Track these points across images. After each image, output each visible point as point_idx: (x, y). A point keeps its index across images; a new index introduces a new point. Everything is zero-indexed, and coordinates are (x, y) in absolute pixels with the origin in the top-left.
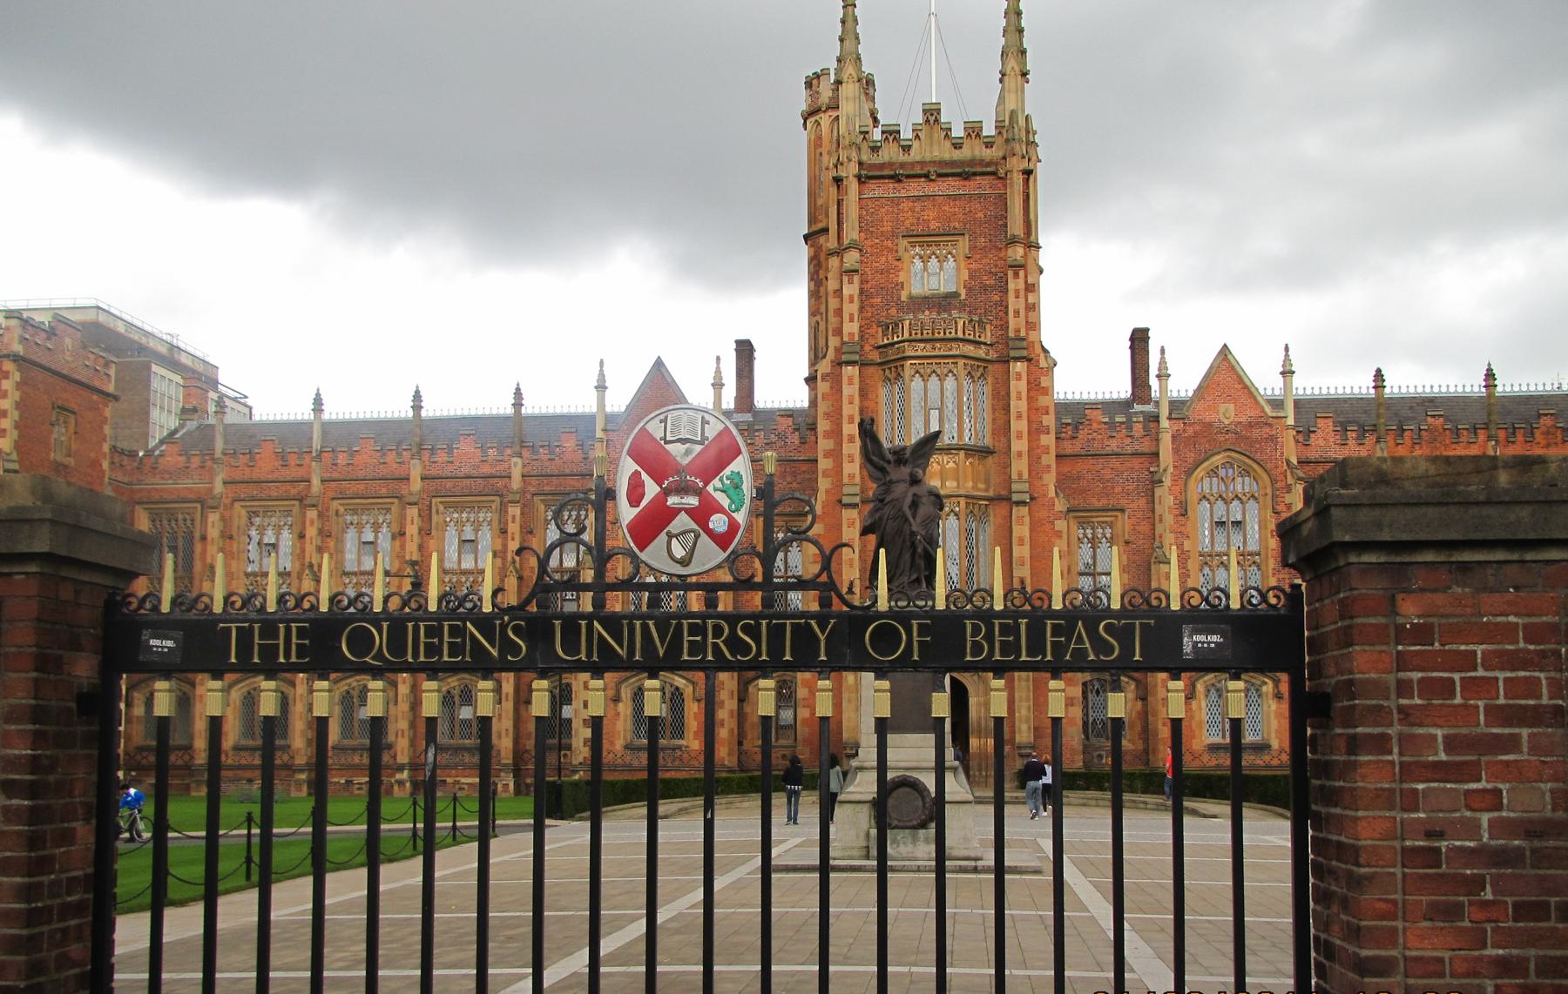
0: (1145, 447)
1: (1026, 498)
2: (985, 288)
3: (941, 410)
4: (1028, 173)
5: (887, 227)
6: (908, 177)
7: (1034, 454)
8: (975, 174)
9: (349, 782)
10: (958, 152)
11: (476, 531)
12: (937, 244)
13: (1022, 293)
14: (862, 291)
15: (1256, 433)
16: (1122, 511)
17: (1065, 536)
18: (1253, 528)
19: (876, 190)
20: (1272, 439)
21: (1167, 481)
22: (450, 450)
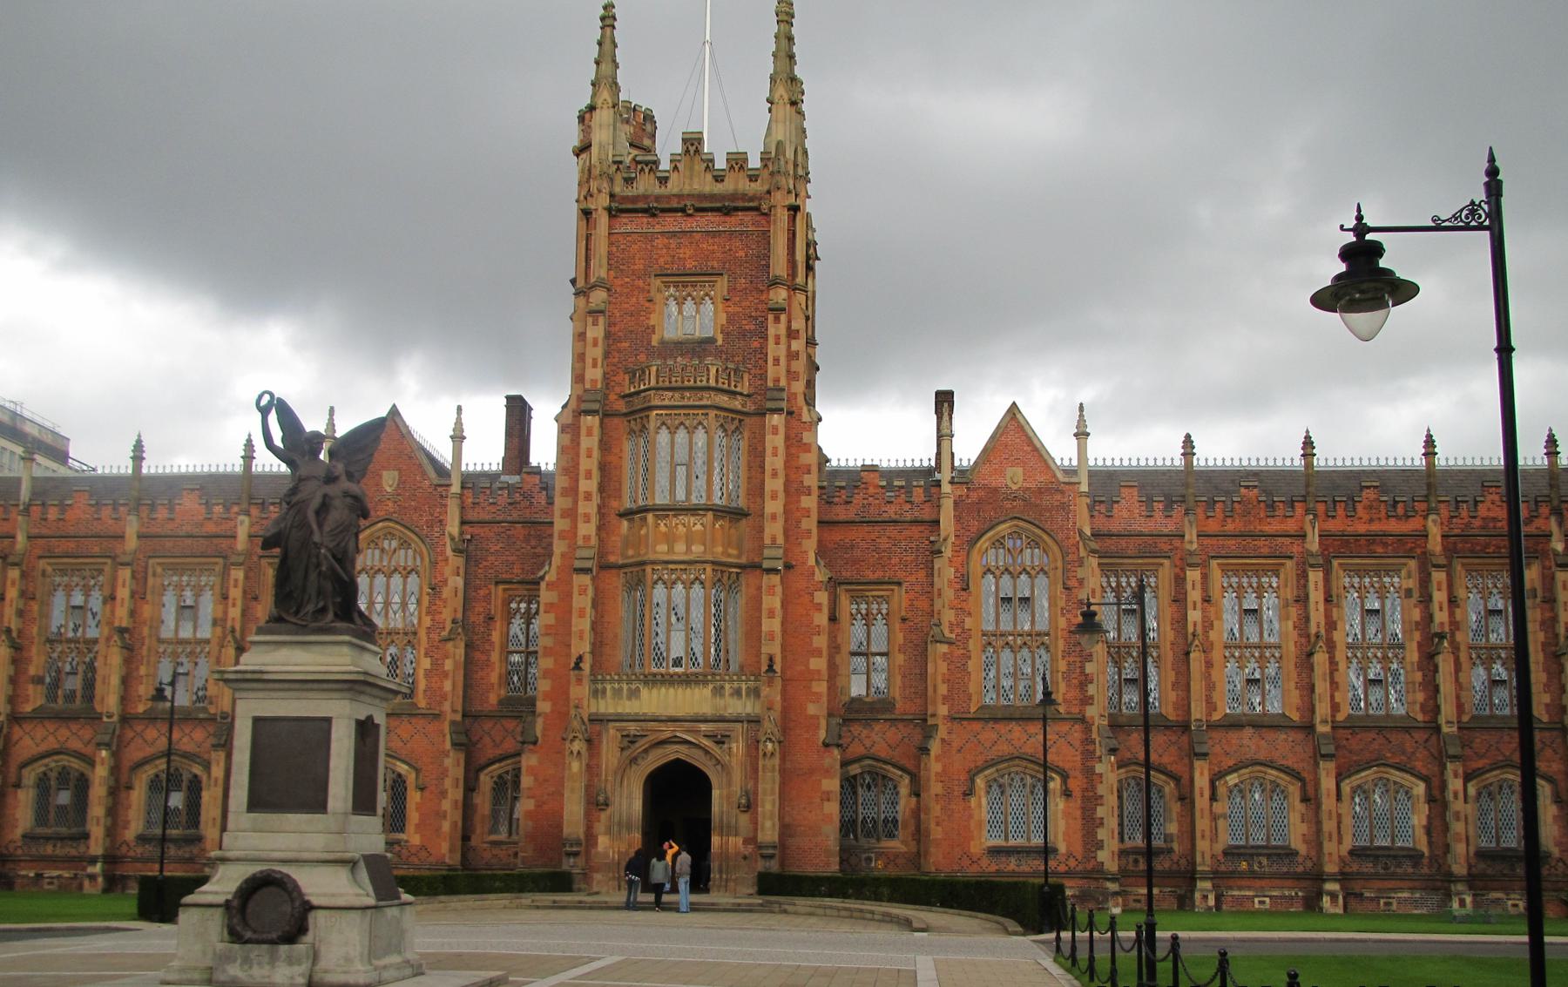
0: (927, 514)
2: (743, 334)
3: (689, 466)
4: (794, 209)
5: (639, 266)
6: (663, 210)
7: (791, 516)
8: (737, 209)
9: (39, 876)
10: (719, 186)
11: (197, 596)
12: (694, 284)
13: (783, 339)
14: (608, 335)
15: (1047, 501)
16: (899, 584)
18: (1042, 603)
19: (627, 224)
20: (1064, 507)
21: (948, 552)
22: (171, 509)
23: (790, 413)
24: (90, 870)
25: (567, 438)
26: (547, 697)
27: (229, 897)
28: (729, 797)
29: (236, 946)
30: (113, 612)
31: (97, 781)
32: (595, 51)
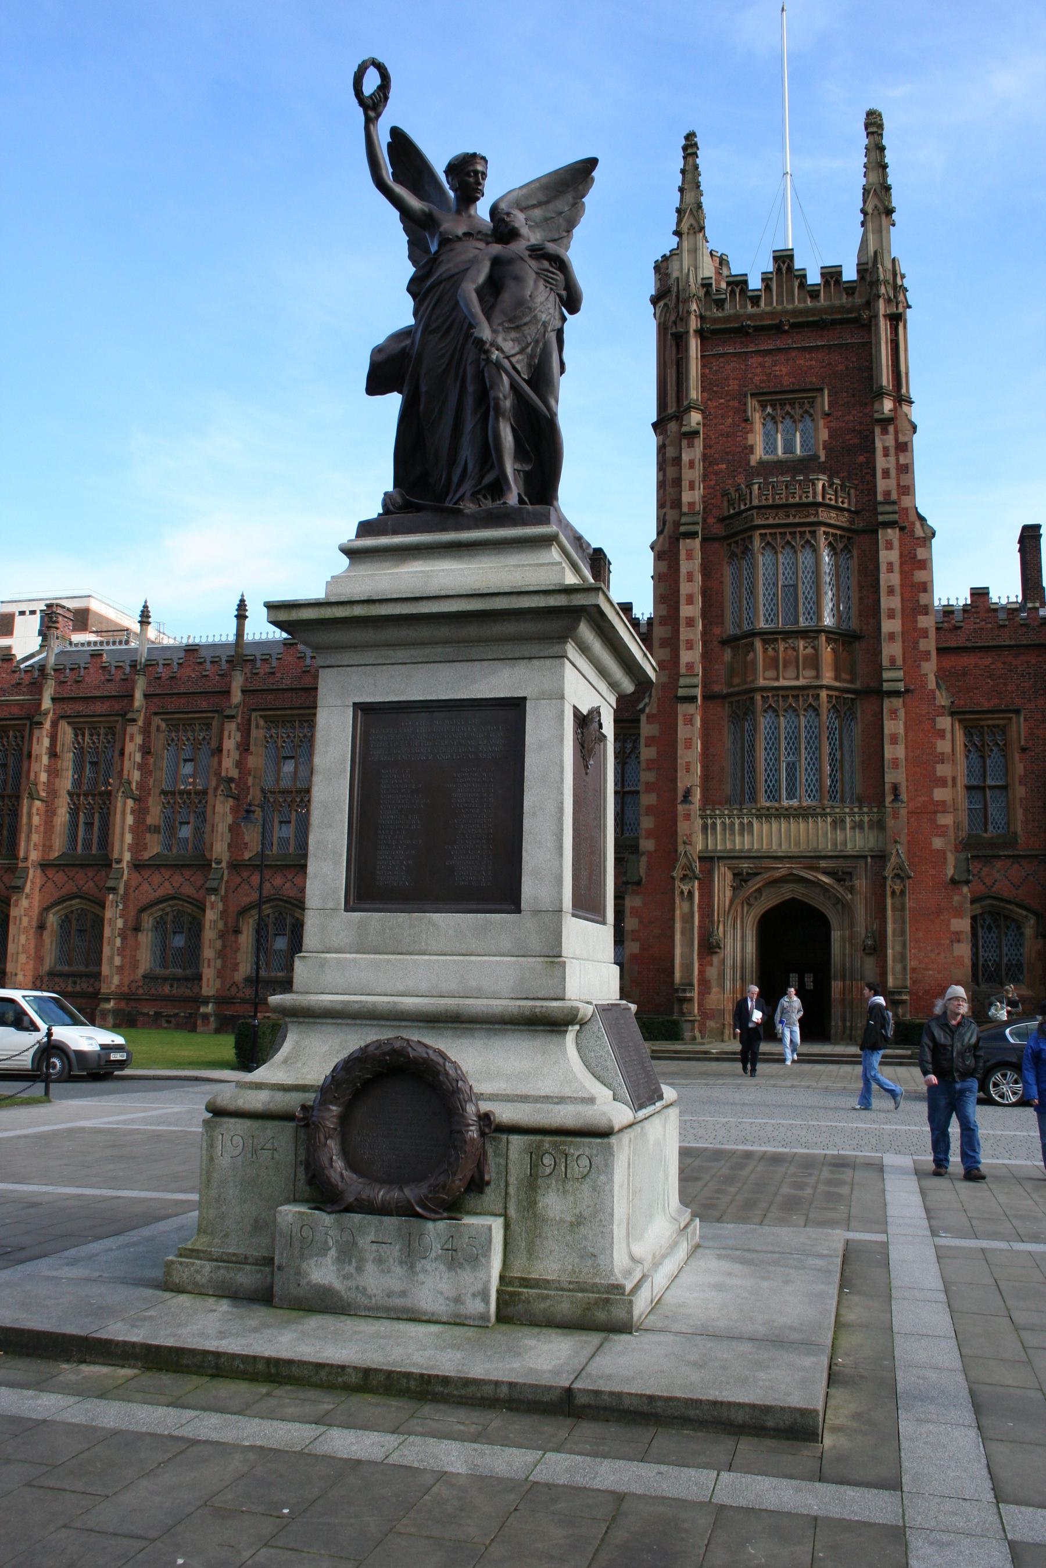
1: (901, 686)
5: (733, 385)
13: (892, 451)
16: (1017, 712)
17: (948, 736)
23: (902, 529)
24: (202, 1010)
25: (664, 564)
26: (650, 834)
27: (310, 1097)
28: (852, 937)
29: (326, 1219)
30: (220, 763)
31: (207, 926)
32: (675, 200)
